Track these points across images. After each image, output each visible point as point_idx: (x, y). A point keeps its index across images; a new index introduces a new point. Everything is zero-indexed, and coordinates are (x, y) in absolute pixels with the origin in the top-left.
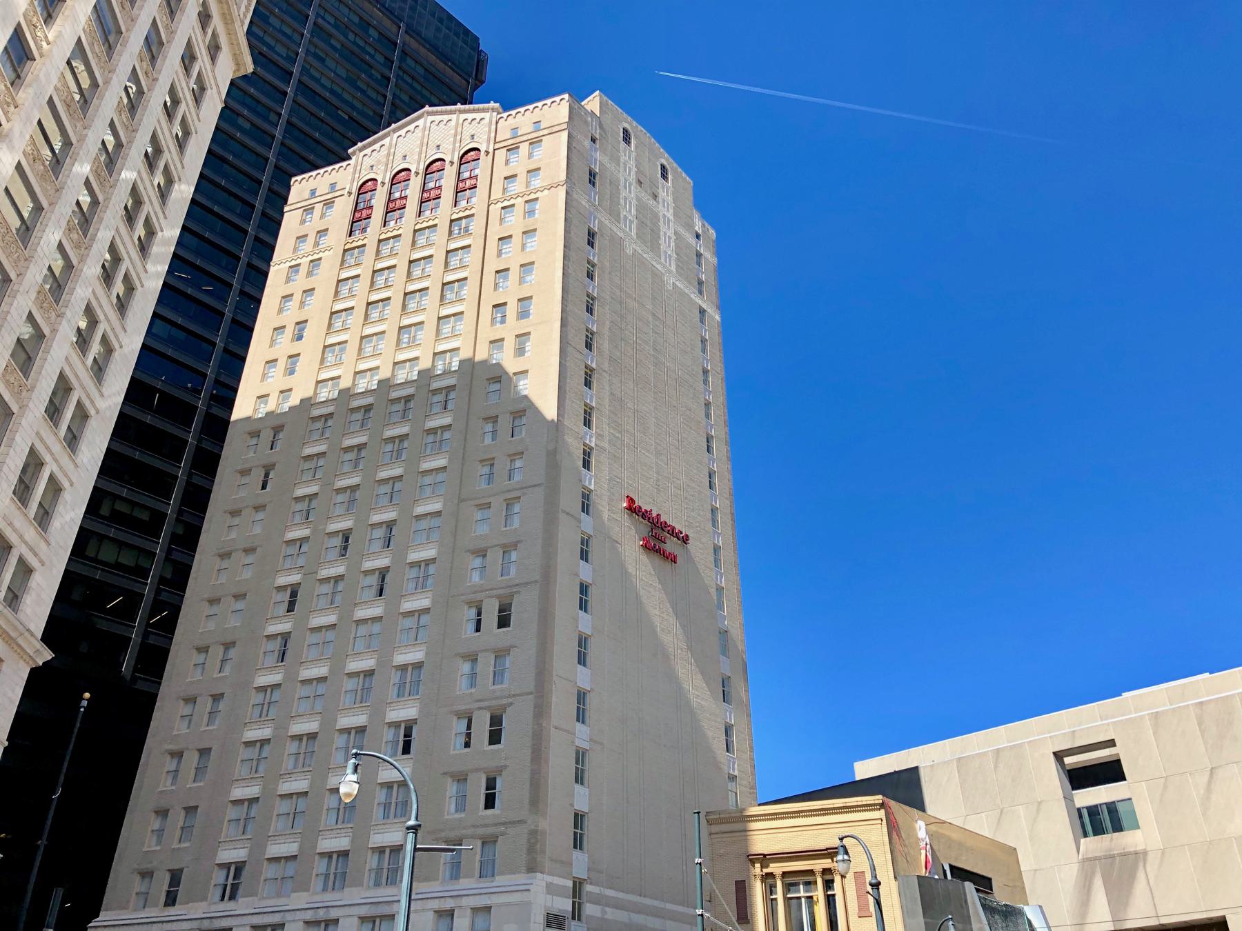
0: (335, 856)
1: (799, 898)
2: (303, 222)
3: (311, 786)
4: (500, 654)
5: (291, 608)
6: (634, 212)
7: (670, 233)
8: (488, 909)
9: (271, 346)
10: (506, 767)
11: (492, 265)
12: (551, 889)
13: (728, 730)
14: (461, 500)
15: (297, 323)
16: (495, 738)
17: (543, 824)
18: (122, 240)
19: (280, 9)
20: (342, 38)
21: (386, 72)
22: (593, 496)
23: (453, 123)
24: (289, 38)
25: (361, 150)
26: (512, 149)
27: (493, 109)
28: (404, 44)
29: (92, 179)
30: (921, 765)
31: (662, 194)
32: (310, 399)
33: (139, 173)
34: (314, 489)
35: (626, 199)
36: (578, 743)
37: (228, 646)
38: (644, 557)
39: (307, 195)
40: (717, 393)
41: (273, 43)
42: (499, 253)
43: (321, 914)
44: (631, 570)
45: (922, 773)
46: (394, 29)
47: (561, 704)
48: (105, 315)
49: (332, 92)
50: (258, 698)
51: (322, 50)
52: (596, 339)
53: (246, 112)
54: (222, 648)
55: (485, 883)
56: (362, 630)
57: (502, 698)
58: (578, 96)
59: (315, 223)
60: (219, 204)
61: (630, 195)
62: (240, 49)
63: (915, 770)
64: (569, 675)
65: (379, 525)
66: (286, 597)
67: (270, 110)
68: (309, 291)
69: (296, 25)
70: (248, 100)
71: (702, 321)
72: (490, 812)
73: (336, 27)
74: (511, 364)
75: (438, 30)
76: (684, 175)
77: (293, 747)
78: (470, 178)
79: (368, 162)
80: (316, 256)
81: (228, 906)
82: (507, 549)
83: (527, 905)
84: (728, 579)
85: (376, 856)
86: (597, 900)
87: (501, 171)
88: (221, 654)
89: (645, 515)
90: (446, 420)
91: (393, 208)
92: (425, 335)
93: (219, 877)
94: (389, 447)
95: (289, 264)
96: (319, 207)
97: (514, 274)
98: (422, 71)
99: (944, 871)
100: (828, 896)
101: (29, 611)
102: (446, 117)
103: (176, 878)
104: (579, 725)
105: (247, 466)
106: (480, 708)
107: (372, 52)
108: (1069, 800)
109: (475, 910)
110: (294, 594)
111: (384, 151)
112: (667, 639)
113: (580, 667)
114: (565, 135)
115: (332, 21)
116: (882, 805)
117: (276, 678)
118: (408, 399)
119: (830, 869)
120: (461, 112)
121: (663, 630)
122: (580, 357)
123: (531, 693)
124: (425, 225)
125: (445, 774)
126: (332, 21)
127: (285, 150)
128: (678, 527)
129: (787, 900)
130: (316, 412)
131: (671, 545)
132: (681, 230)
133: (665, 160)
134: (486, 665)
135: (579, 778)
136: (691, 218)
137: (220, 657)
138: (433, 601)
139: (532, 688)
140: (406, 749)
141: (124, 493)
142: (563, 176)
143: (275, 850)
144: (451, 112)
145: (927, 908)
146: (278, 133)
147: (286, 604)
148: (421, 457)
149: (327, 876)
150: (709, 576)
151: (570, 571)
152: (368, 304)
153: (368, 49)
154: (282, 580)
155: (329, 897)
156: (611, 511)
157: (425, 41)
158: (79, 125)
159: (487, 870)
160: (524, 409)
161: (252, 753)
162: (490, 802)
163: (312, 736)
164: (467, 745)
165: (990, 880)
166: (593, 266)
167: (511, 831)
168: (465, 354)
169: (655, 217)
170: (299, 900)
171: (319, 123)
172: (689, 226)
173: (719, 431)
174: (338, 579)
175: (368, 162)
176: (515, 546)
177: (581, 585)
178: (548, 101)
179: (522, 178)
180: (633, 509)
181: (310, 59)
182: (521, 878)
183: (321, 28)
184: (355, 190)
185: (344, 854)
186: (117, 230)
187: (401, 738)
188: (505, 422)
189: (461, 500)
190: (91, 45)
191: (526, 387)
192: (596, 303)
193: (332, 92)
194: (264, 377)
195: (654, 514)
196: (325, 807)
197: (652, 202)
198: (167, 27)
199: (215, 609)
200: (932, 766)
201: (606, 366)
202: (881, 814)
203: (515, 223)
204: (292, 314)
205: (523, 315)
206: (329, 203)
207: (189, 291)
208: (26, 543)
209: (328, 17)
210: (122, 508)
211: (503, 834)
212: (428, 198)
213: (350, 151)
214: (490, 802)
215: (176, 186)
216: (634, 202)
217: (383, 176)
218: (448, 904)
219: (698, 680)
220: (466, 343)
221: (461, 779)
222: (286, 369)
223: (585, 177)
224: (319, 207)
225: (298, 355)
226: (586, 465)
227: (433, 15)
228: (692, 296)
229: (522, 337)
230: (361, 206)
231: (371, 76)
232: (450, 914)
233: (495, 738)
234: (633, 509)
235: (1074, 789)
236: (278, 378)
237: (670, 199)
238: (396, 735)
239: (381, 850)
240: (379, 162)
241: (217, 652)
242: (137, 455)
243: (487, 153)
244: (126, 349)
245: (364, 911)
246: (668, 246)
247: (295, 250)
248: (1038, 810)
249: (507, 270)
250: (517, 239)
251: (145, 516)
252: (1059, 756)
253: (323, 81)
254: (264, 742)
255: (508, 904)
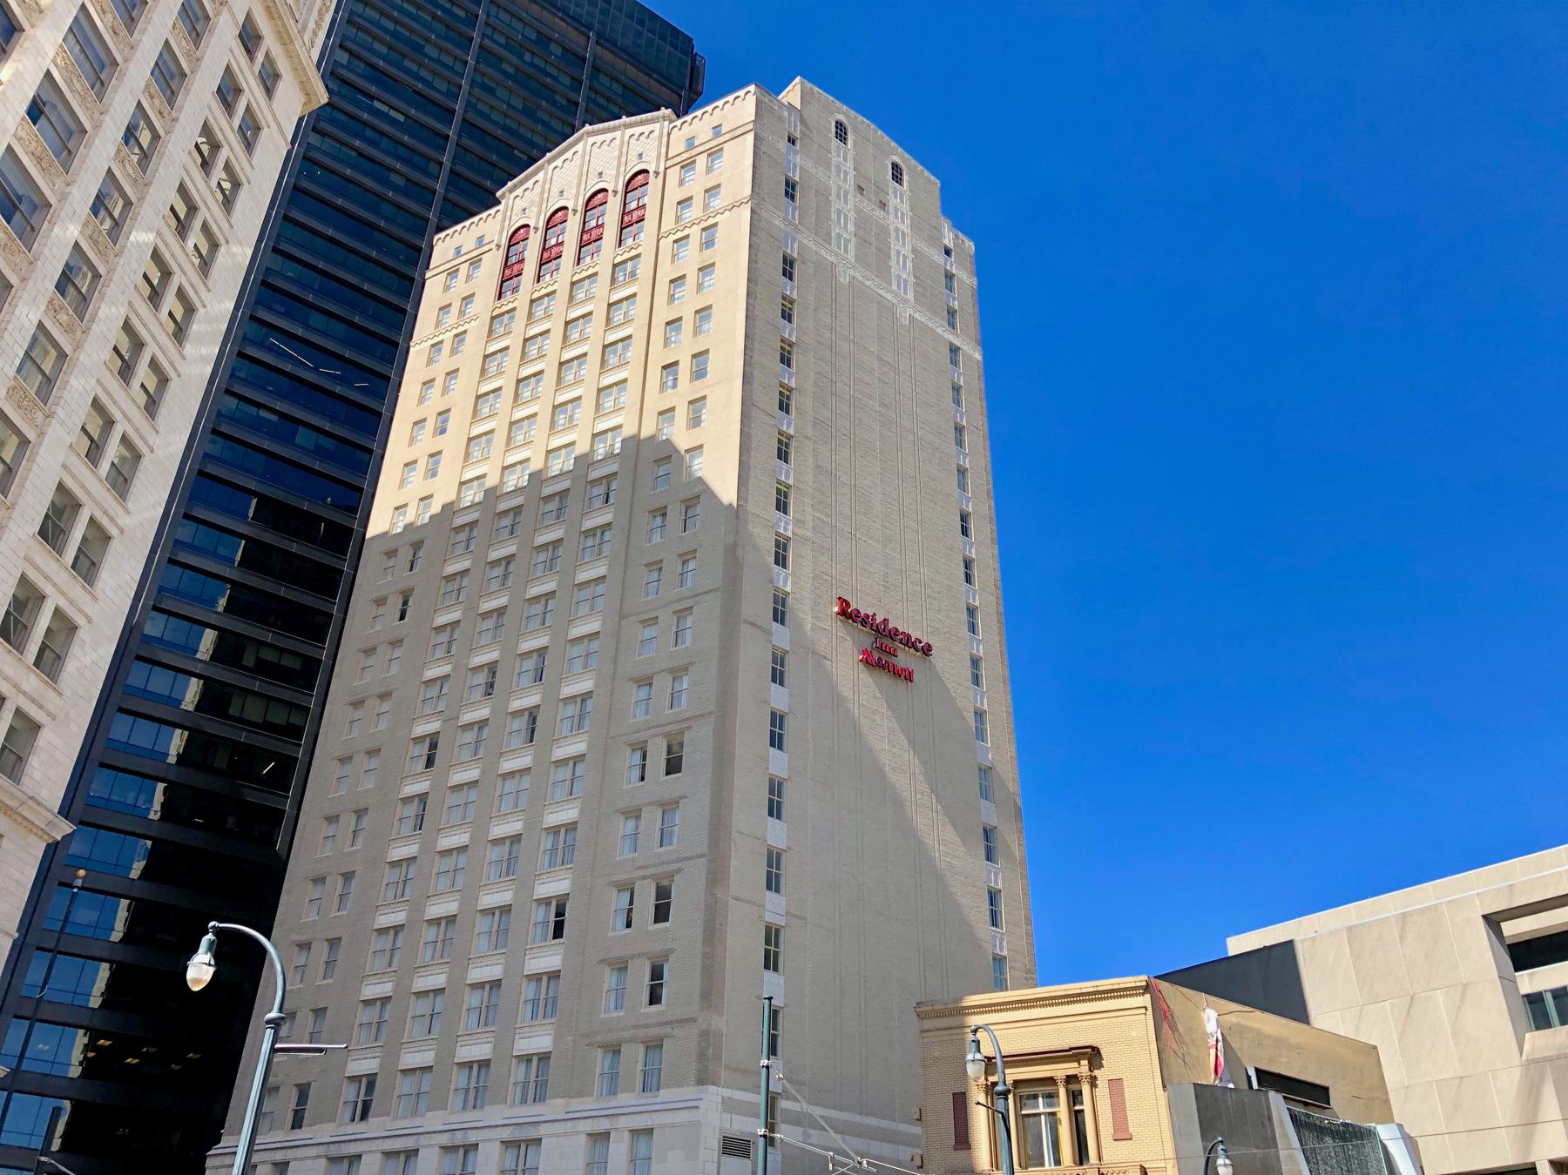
0: (475, 1067)
1: (1039, 1115)
2: (447, 288)
3: (449, 980)
4: (669, 806)
5: (430, 762)
6: (851, 227)
7: (906, 250)
8: (649, 1132)
9: (411, 444)
10: (673, 950)
11: (663, 314)
12: (729, 1106)
13: (993, 897)
14: (622, 617)
15: (440, 414)
16: (662, 914)
17: (718, 1023)
18: (141, 320)
19: (438, 35)
20: (515, 60)
21: (573, 95)
22: (790, 601)
23: (617, 142)
24: (450, 68)
25: (511, 191)
26: (688, 165)
27: (664, 118)
28: (595, 57)
29: (85, 246)
30: (1298, 939)
31: (893, 202)
32: (452, 504)
33: (159, 234)
34: (455, 615)
35: (839, 212)
36: (769, 918)
37: (360, 813)
38: (866, 678)
39: (451, 254)
40: (977, 456)
41: (429, 77)
42: (671, 299)
43: (459, 1138)
44: (846, 692)
45: (1300, 950)
46: (582, 40)
47: (746, 869)
48: (123, 413)
49: (505, 128)
50: (392, 875)
51: (491, 79)
52: (794, 397)
53: (398, 166)
54: (354, 817)
55: (647, 1099)
56: (510, 786)
57: (670, 862)
58: (772, 85)
59: (460, 287)
60: (371, 281)
61: (846, 209)
62: (306, 75)
63: (1289, 944)
64: (754, 832)
65: (529, 654)
66: (424, 750)
67: (429, 159)
68: (452, 373)
69: (458, 52)
70: (401, 151)
71: (954, 362)
72: (655, 1008)
73: (506, 47)
74: (682, 438)
75: (638, 34)
76: (927, 173)
77: (430, 934)
78: (638, 208)
79: (520, 204)
80: (461, 329)
81: (359, 1128)
82: (677, 673)
83: (697, 1124)
84: (995, 698)
85: (523, 1066)
86: (797, 1120)
87: (674, 194)
88: (353, 823)
89: (865, 621)
90: (606, 517)
91: (549, 257)
92: (584, 413)
93: (350, 1093)
94: (542, 557)
95: (431, 342)
96: (464, 268)
97: (687, 325)
98: (620, 90)
99: (1249, 1077)
100: (1077, 1112)
101: (37, 775)
102: (609, 136)
103: (303, 1092)
104: (770, 895)
105: (383, 593)
106: (643, 878)
107: (554, 72)
108: (1509, 985)
109: (635, 1133)
110: (433, 746)
111: (538, 188)
112: (901, 782)
113: (772, 821)
114: (750, 137)
115: (502, 40)
116: (1147, 989)
117: (411, 850)
118: (563, 494)
119: (1075, 1076)
120: (626, 126)
121: (894, 769)
122: (771, 421)
123: (703, 856)
124: (584, 274)
125: (602, 961)
126: (502, 40)
127: (449, 206)
128: (914, 635)
129: (1022, 1118)
130: (459, 521)
131: (904, 659)
132: (922, 246)
133: (899, 156)
134: (652, 819)
135: (771, 962)
136: (938, 229)
137: (352, 828)
138: (590, 746)
139: (704, 849)
140: (558, 931)
141: (269, 638)
142: (748, 191)
143: (410, 1059)
144: (614, 129)
145: (1207, 1129)
146: (439, 187)
147: (424, 759)
148: (576, 567)
149: (467, 1090)
150: (965, 697)
151: (756, 698)
152: (600, 390)
153: (550, 69)
154: (421, 729)
155: (471, 1116)
156: (815, 619)
157: (620, 51)
158: (59, 182)
159: (650, 1083)
160: (698, 496)
161: (385, 942)
162: (655, 998)
163: (451, 919)
164: (629, 925)
165: (1326, 1089)
166: (791, 302)
167: (678, 1032)
168: (629, 430)
169: (883, 232)
170: (434, 1120)
171: (491, 168)
172: (934, 240)
173: (981, 506)
174: (482, 723)
175: (520, 204)
176: (685, 669)
177: (773, 714)
178: (730, 98)
179: (698, 202)
180: (847, 613)
181: (476, 91)
182: (690, 1092)
183: (490, 52)
184: (504, 241)
185: (484, 1064)
186: (130, 304)
187: (552, 918)
188: (675, 515)
189: (622, 617)
190: (69, 83)
191: (702, 467)
192: (795, 349)
193: (505, 128)
194: (403, 483)
195: (879, 619)
196: (465, 1006)
197: (879, 213)
198: (188, 54)
199: (347, 770)
200: (1313, 939)
201: (809, 431)
202: (1146, 1000)
203: (692, 256)
204: (435, 401)
205: (699, 374)
206: (475, 262)
207: (338, 389)
208: (25, 693)
209: (496, 37)
210: (269, 656)
211: (669, 1036)
212: (589, 239)
213: (498, 194)
214: (655, 998)
215: (222, 250)
216: (852, 215)
217: (537, 220)
218: (603, 1125)
219: (949, 833)
220: (627, 419)
221: (621, 967)
222: (427, 471)
223: (779, 188)
224: (464, 268)
225: (440, 452)
226: (781, 560)
227: (631, 17)
228: (939, 330)
229: (697, 402)
230: (513, 260)
231: (554, 103)
232: (606, 1135)
233: (662, 914)
234: (847, 613)
235: (1517, 970)
236: (418, 484)
237: (906, 207)
238: (547, 912)
239: (527, 1059)
240: (532, 202)
241: (349, 821)
242: (283, 592)
243: (657, 173)
244: (160, 453)
245: (506, 1134)
246: (902, 267)
247: (438, 323)
248: (1464, 995)
249: (680, 319)
250: (691, 281)
251: (292, 663)
252: (1493, 921)
253: (496, 116)
254: (398, 929)
255: (673, 1126)
